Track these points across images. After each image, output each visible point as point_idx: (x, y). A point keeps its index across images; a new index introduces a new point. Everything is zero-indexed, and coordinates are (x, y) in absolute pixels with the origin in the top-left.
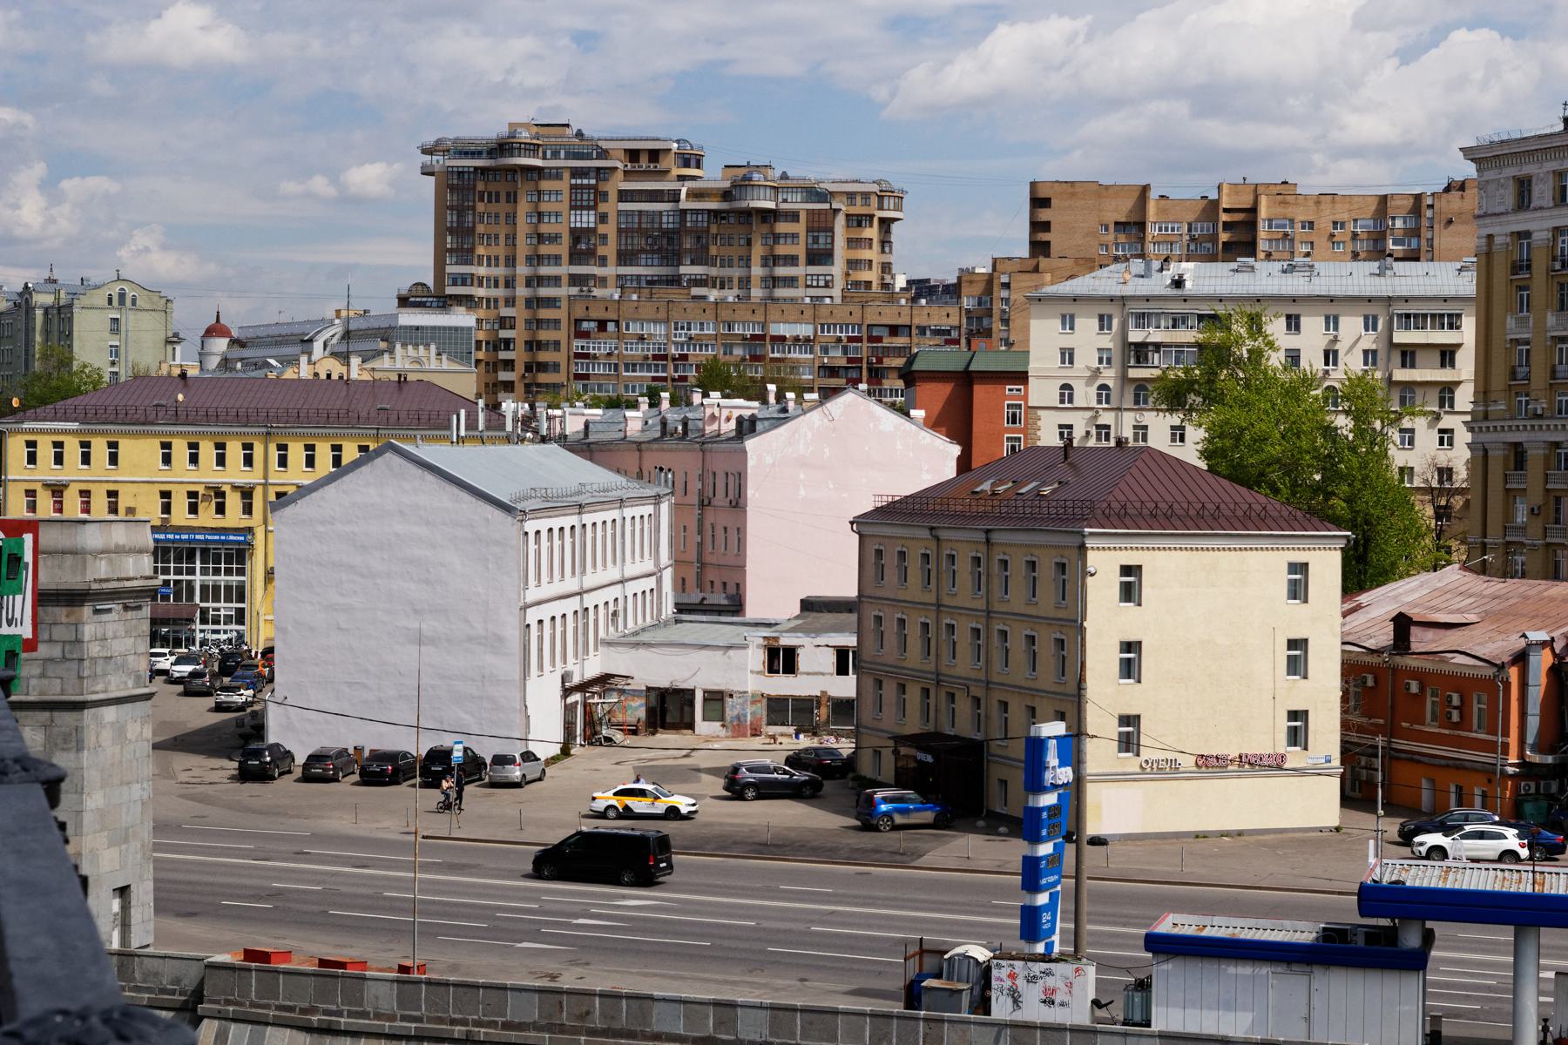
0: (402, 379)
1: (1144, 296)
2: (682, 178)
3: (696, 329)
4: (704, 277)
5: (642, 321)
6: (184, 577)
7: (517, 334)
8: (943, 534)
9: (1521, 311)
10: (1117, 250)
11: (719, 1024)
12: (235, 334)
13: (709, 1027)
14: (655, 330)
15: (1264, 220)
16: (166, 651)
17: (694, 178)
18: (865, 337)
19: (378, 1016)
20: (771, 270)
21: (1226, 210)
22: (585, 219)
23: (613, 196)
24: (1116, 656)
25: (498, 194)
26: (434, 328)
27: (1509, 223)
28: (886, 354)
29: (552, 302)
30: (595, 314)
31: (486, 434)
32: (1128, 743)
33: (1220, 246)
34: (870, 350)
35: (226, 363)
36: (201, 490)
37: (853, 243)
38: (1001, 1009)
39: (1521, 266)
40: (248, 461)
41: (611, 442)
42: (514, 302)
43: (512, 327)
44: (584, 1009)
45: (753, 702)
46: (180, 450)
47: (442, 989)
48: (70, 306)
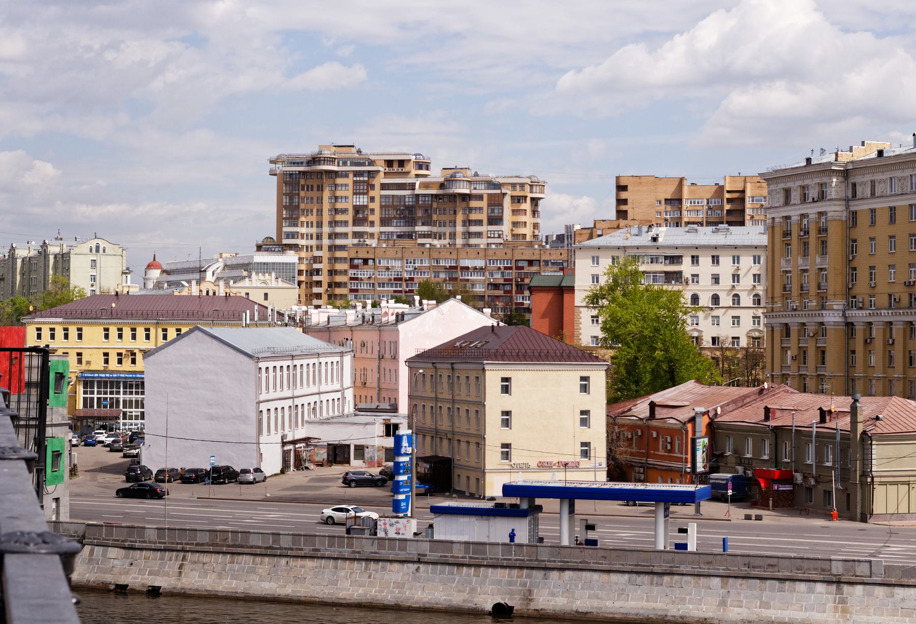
0: (228, 295)
1: (636, 246)
2: (417, 176)
3: (418, 263)
4: (429, 233)
5: (388, 259)
6: (115, 396)
7: (324, 266)
8: (438, 366)
9: (788, 257)
10: (666, 215)
11: (274, 541)
12: (165, 268)
13: (270, 543)
14: (395, 264)
15: (749, 197)
16: (104, 431)
17: (425, 176)
18: (514, 268)
19: (150, 542)
20: (468, 229)
21: (728, 192)
22: (361, 200)
23: (377, 187)
24: (499, 417)
25: (312, 186)
26: (274, 263)
27: (781, 212)
28: (526, 276)
29: (342, 248)
30: (360, 256)
31: (258, 322)
32: (506, 456)
33: (725, 212)
34: (517, 274)
35: (158, 285)
36: (124, 352)
37: (515, 212)
38: (380, 534)
39: (787, 234)
40: (148, 337)
41: (338, 327)
42: (322, 248)
43: (321, 262)
44: (225, 537)
45: (378, 451)
46: (113, 332)
47: (174, 531)
48: (69, 254)
